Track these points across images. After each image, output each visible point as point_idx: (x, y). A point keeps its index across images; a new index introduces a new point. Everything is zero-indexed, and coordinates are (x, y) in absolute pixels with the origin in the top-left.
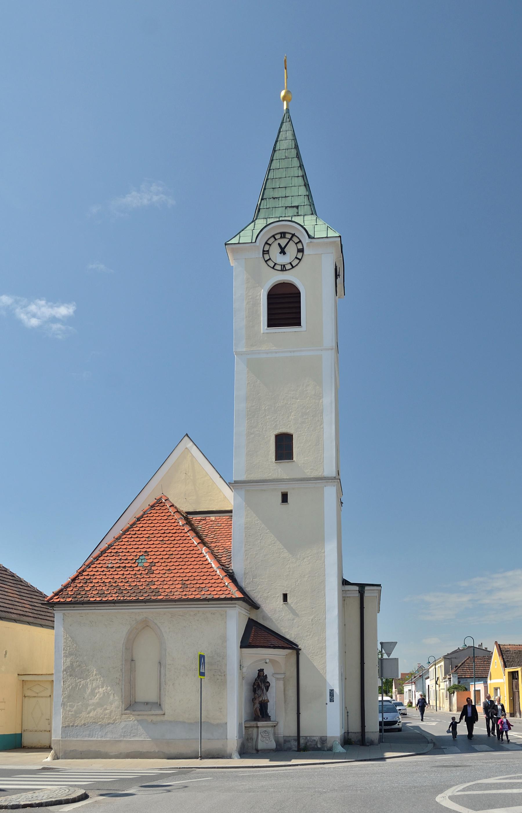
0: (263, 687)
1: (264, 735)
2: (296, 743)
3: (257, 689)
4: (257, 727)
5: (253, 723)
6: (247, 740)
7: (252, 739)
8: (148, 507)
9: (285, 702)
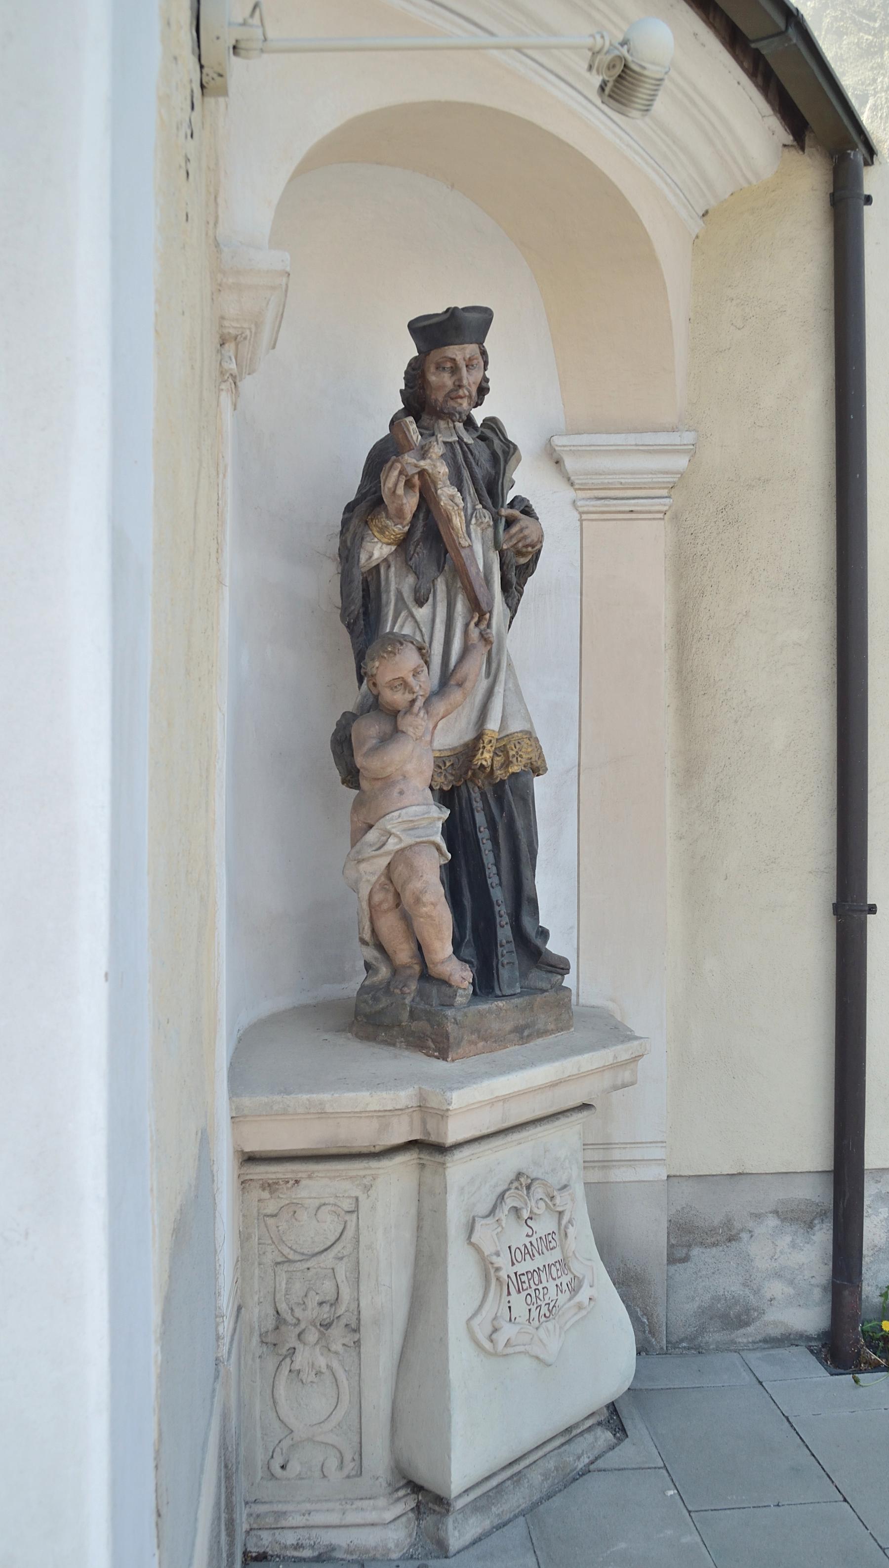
0: (477, 547)
1: (502, 1237)
2: (811, 1255)
3: (398, 584)
4: (429, 1148)
5: (376, 1093)
6: (277, 1338)
7: (341, 1324)
8: (344, 1545)
9: (691, 770)
